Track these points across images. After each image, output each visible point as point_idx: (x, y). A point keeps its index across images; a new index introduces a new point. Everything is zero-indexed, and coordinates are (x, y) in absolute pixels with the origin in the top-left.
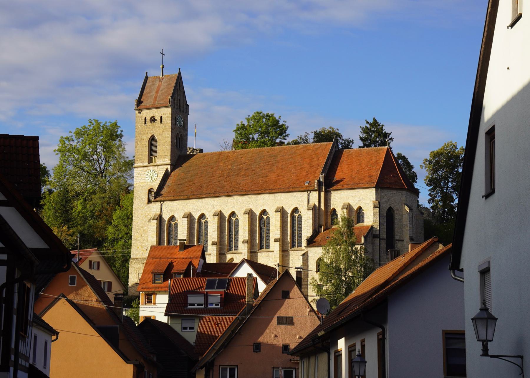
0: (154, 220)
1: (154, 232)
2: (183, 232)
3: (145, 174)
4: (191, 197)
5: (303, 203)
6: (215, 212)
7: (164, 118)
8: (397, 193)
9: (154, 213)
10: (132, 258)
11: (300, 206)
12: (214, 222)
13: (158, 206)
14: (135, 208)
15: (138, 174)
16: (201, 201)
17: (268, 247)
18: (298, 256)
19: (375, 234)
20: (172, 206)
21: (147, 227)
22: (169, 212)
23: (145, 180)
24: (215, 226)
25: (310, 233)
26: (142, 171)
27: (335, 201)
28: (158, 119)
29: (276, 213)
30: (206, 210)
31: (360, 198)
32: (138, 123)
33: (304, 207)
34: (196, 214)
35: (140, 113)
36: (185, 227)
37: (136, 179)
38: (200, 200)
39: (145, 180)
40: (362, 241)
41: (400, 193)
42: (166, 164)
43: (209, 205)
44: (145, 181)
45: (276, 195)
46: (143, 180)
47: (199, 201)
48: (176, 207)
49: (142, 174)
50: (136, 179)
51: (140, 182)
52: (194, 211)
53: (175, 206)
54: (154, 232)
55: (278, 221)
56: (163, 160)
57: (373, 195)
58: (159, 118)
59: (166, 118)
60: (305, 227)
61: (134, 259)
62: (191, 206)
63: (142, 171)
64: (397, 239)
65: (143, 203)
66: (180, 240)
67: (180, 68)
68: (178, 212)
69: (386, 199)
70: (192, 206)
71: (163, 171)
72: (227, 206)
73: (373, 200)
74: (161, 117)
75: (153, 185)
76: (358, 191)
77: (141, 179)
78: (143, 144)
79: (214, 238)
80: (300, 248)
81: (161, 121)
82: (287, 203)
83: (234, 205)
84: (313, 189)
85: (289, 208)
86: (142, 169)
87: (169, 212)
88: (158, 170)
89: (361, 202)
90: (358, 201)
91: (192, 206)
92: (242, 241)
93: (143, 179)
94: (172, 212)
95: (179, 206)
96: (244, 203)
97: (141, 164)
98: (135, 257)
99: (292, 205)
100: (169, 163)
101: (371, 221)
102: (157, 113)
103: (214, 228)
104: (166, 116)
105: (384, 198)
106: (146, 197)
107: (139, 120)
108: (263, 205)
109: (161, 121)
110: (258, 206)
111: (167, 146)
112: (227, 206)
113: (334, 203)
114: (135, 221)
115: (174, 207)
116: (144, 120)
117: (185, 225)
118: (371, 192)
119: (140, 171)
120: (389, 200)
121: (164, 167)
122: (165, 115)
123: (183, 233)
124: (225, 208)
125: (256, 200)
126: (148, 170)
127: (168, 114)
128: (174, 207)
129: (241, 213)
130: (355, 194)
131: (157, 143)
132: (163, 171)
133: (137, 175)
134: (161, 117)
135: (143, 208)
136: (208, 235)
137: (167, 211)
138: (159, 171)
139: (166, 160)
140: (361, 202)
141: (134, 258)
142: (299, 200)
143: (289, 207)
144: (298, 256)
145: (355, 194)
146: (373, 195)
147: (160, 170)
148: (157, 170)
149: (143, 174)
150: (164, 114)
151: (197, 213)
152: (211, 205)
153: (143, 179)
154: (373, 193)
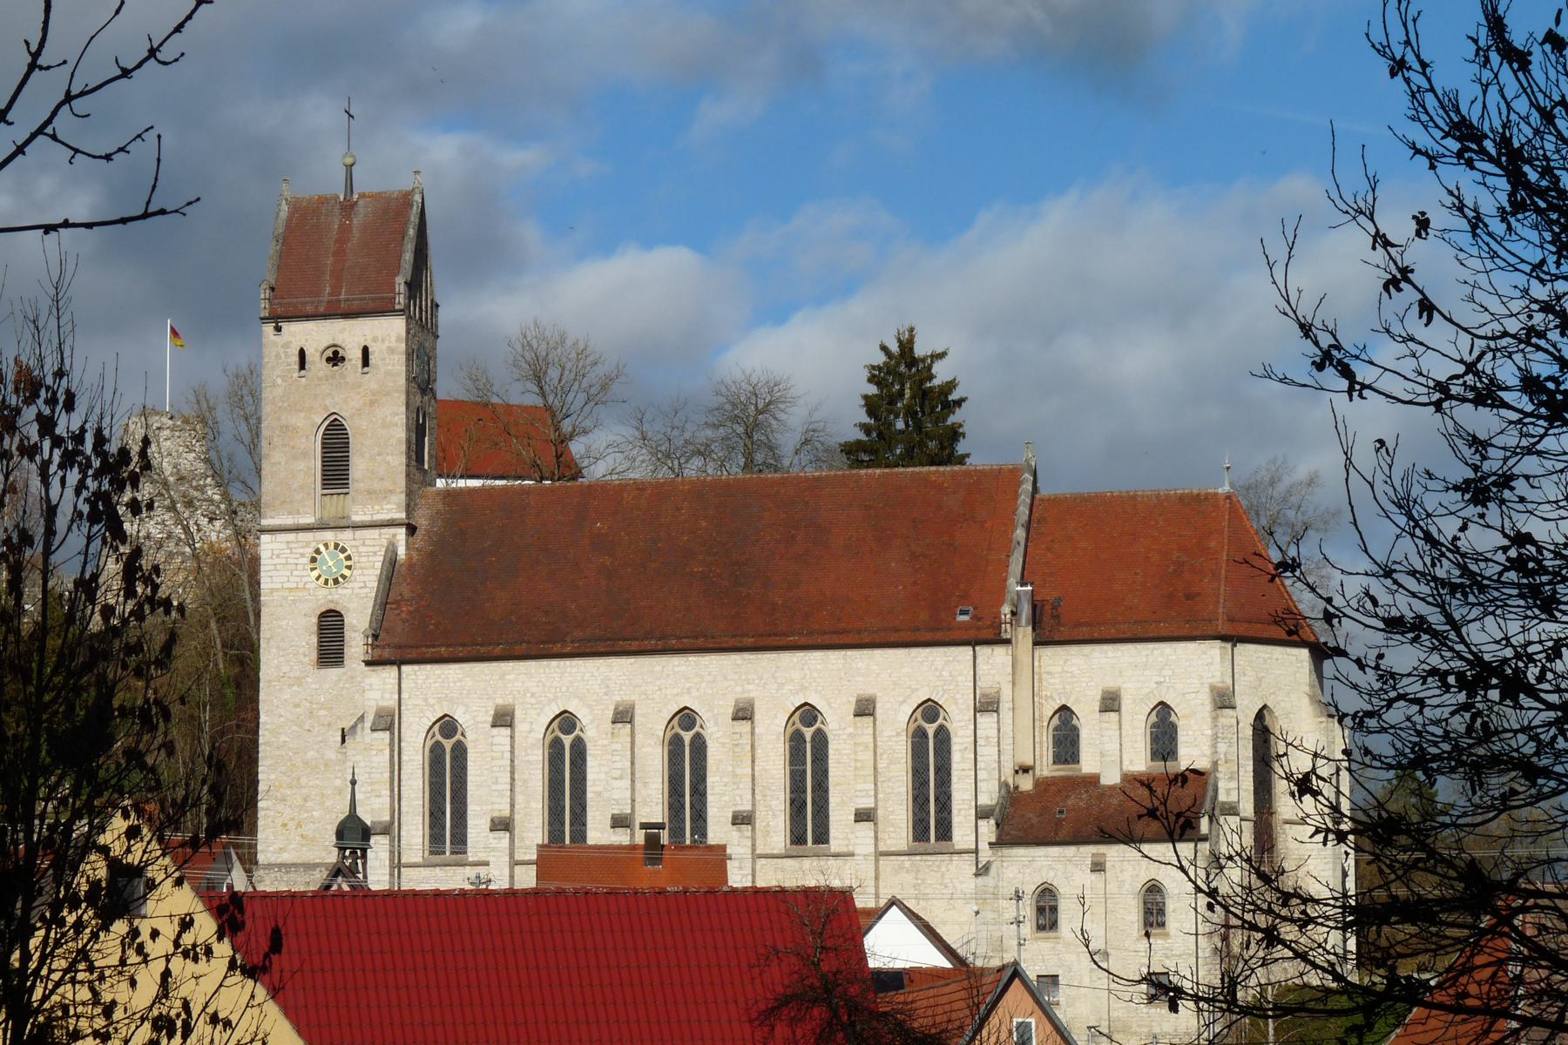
0: (380, 733)
1: (379, 775)
2: (497, 778)
3: (303, 555)
4: (518, 649)
5: (957, 685)
6: (616, 709)
7: (376, 354)
8: (1285, 656)
9: (373, 704)
10: (260, 862)
11: (946, 696)
12: (618, 746)
13: (387, 681)
14: (269, 681)
15: (278, 556)
16: (558, 667)
17: (822, 837)
18: (939, 875)
19: (1226, 803)
20: (443, 682)
21: (317, 751)
22: (431, 701)
23: (304, 579)
24: (621, 761)
25: (991, 793)
26: (293, 545)
27: (1070, 680)
28: (355, 355)
29: (858, 719)
30: (577, 701)
31: (1164, 672)
32: (272, 368)
33: (960, 701)
34: (539, 714)
35: (278, 329)
36: (502, 758)
37: (269, 574)
38: (554, 663)
39: (304, 579)
40: (1202, 828)
41: (1294, 658)
42: (288, 527)
43: (591, 682)
44: (305, 583)
45: (850, 653)
46: (298, 579)
47: (549, 665)
48: (458, 684)
49: (292, 556)
50: (269, 574)
51: (286, 585)
52: (533, 701)
53: (455, 682)
54: (382, 773)
55: (867, 747)
56: (377, 507)
57: (1211, 664)
58: (359, 354)
59: (386, 355)
60: (963, 770)
61: (270, 866)
62: (520, 684)
63: (293, 545)
64: (1287, 817)
65: (302, 663)
66: (644, 826)
67: (187, 217)
68: (466, 706)
69: (1251, 679)
70: (523, 682)
71: (377, 548)
72: (660, 689)
73: (1210, 681)
74: (365, 351)
75: (337, 596)
76: (1154, 649)
77: (288, 573)
78: (293, 447)
79: (618, 804)
80: (944, 843)
81: (366, 361)
82: (895, 683)
83: (687, 685)
84: (992, 637)
85: (904, 701)
86: (291, 536)
87: (431, 701)
88: (357, 543)
89: (1168, 688)
90: (1157, 683)
91: (523, 682)
92: (730, 815)
93: (295, 573)
94: (445, 703)
95: (470, 684)
96: (729, 677)
97: (288, 521)
98: (273, 859)
99: (914, 690)
100: (401, 522)
101: (1205, 756)
102: (351, 334)
103: (618, 765)
104: (384, 347)
105: (1245, 675)
106: (676, 663)
107: (278, 356)
108: (803, 688)
109: (366, 361)
110: (784, 691)
111: (389, 458)
112: (660, 689)
113: (1064, 689)
114: (267, 727)
115: (452, 685)
116: (296, 359)
117: (503, 752)
118: (1205, 653)
119: (284, 546)
120: (1260, 680)
121: (380, 534)
122: (379, 343)
123: (496, 783)
124: (655, 696)
125: (776, 671)
126: (318, 542)
127: (393, 339)
128: (452, 685)
129: (714, 715)
130: (1144, 659)
131: (348, 443)
132: (377, 548)
133: (271, 558)
134: (365, 351)
135: (299, 681)
136: (589, 789)
137: (426, 700)
138: (362, 549)
139: (389, 506)
140: (1168, 688)
141: (269, 865)
142: (941, 675)
143: (901, 699)
144: (939, 875)
145: (1144, 659)
146: (1211, 664)
147: (364, 545)
148: (353, 543)
149: (298, 556)
150: (375, 339)
151: (542, 709)
152: (599, 682)
153: (285, 579)
154: (1212, 658)
